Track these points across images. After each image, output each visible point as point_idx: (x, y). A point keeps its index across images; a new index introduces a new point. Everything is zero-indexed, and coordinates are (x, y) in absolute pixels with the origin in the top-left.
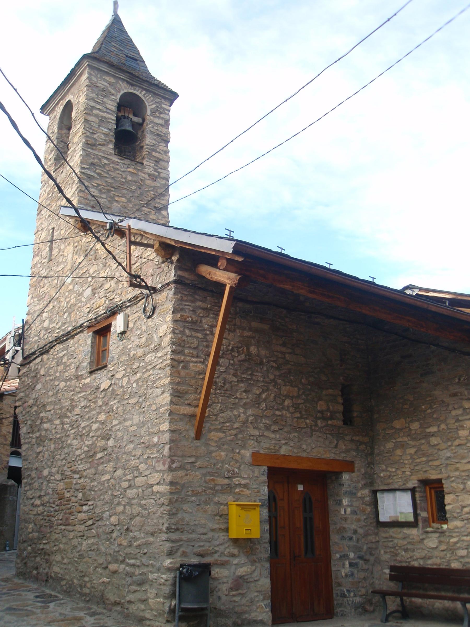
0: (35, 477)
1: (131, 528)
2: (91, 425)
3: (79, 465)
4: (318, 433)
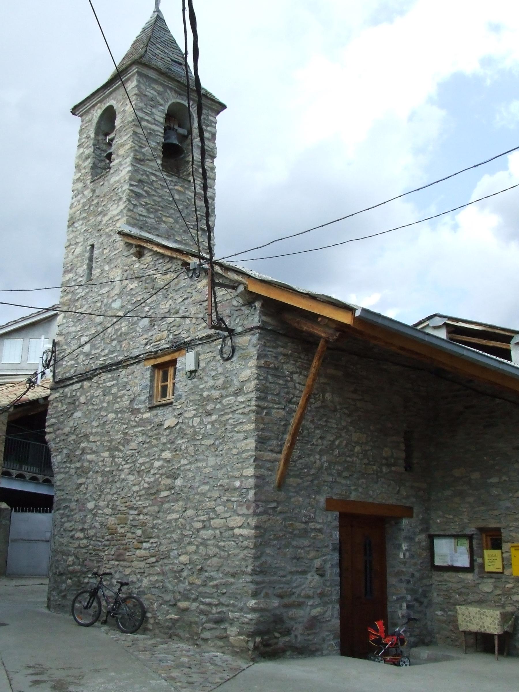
0: (75, 509)
1: (206, 568)
2: (153, 461)
3: (137, 501)
4: (383, 479)
